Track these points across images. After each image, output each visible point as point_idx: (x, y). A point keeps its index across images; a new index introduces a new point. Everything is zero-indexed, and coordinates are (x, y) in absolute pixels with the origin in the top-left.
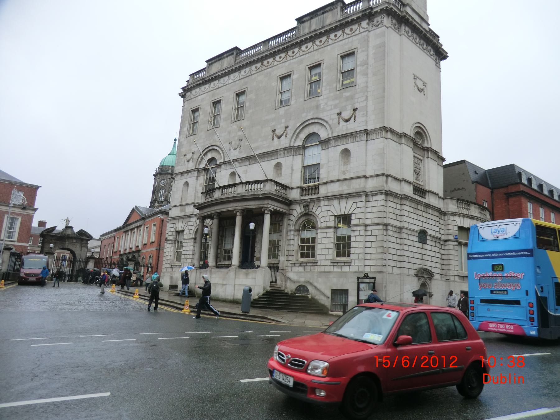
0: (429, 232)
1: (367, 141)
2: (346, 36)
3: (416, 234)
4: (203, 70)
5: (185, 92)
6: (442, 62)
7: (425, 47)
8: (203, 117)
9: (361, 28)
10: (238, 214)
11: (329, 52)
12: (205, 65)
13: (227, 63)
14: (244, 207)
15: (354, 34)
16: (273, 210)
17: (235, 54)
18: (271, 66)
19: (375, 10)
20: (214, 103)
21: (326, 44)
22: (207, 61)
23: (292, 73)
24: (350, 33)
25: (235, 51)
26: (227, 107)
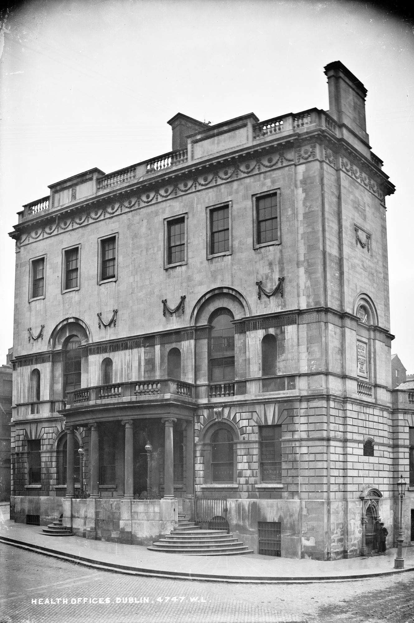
0: (377, 440)
1: (86, 517)
2: (160, 199)
3: (362, 446)
4: (46, 199)
5: (18, 234)
6: (387, 198)
7: (367, 182)
8: (54, 274)
9: (45, 234)
10: (127, 426)
11: (86, 239)
12: (47, 192)
13: (87, 192)
14: (136, 417)
15: (274, 167)
16: (176, 420)
17: (95, 178)
18: (153, 202)
19: (302, 137)
20: (66, 252)
21: (153, 202)
22: (51, 187)
23: (186, 216)
24: (268, 164)
25: (94, 175)
26: (89, 263)
